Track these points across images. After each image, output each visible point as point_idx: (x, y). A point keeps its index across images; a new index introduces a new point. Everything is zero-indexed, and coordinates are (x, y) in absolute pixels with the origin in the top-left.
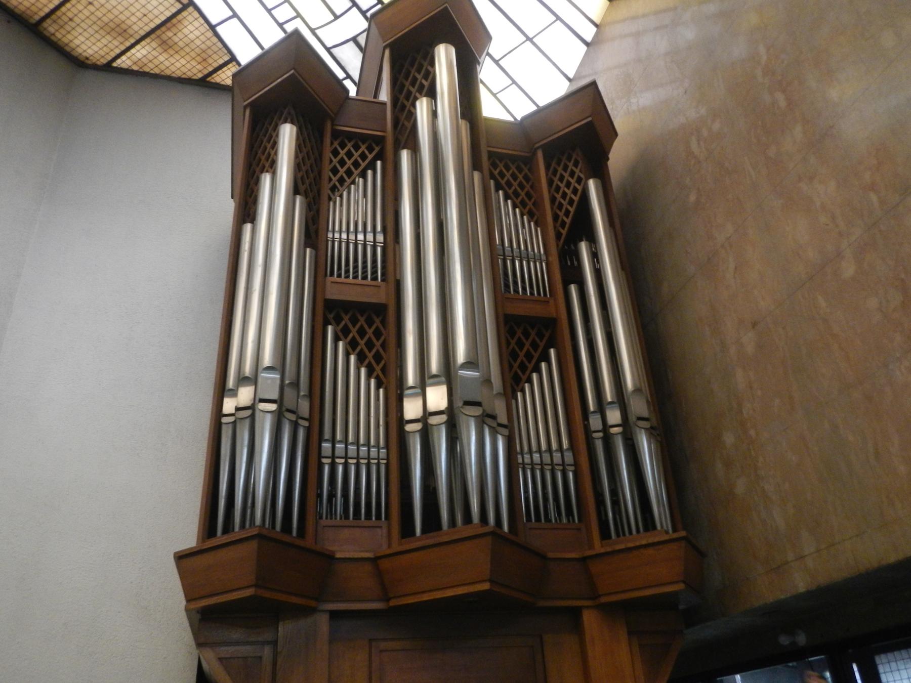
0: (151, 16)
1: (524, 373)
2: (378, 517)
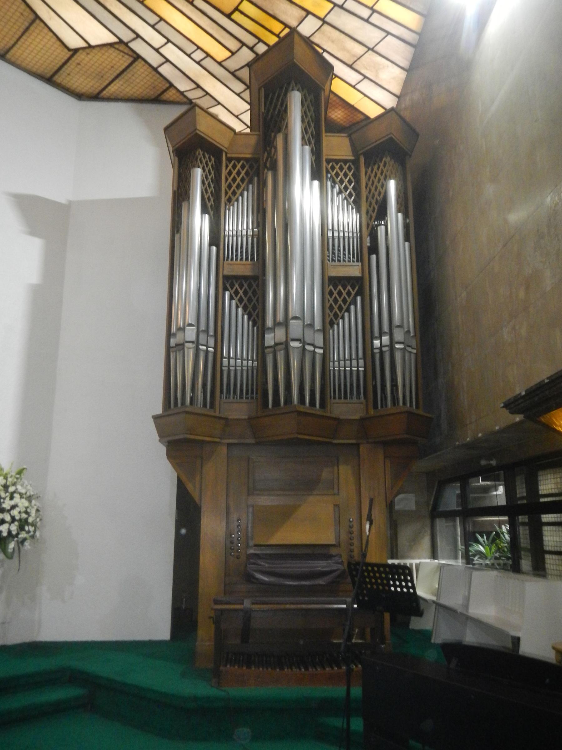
0: (116, 67)
1: (340, 312)
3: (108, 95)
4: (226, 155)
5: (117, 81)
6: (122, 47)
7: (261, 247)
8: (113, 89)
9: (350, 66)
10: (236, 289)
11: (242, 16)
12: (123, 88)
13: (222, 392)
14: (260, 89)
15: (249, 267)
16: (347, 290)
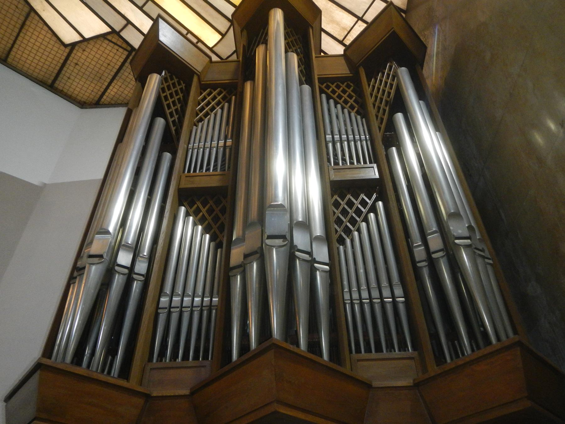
0: (112, 64)
3: (108, 100)
5: (115, 81)
6: (115, 39)
8: (112, 91)
12: (121, 89)
14: (242, 31)
16: (360, 199)
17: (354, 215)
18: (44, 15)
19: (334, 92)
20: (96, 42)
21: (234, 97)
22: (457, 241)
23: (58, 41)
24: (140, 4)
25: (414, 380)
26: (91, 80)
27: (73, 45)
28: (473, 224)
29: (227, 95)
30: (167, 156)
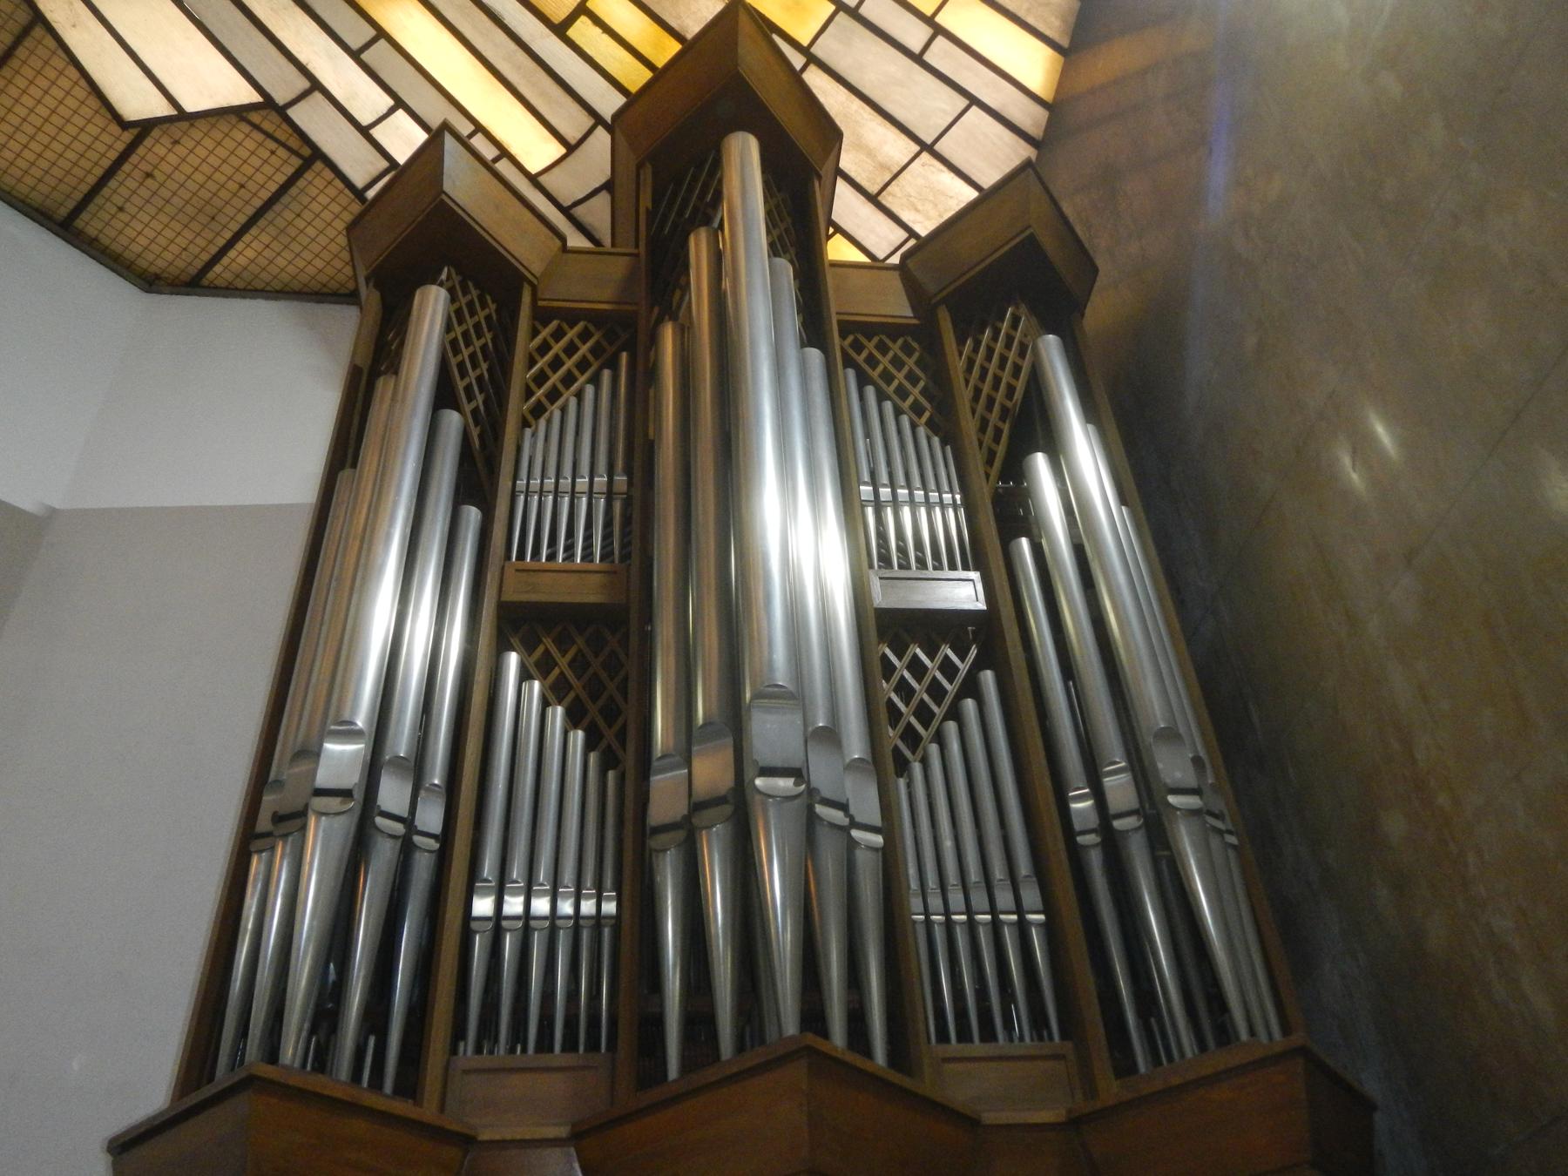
0: (251, 186)
2: (593, 1046)
3: (228, 276)
4: (535, 298)
5: (254, 231)
6: (270, 122)
7: (636, 527)
8: (242, 255)
9: (873, 199)
10: (547, 651)
11: (598, 30)
13: (459, 1033)
14: (640, 167)
15: (596, 579)
16: (939, 658)
17: (907, 675)
18: (72, 39)
19: (872, 361)
20: (213, 126)
21: (624, 355)
22: (1171, 799)
23: (103, 111)
24: (355, 45)
25: (1069, 1111)
26: (186, 220)
27: (146, 127)
28: (1202, 754)
29: (605, 344)
30: (472, 515)
